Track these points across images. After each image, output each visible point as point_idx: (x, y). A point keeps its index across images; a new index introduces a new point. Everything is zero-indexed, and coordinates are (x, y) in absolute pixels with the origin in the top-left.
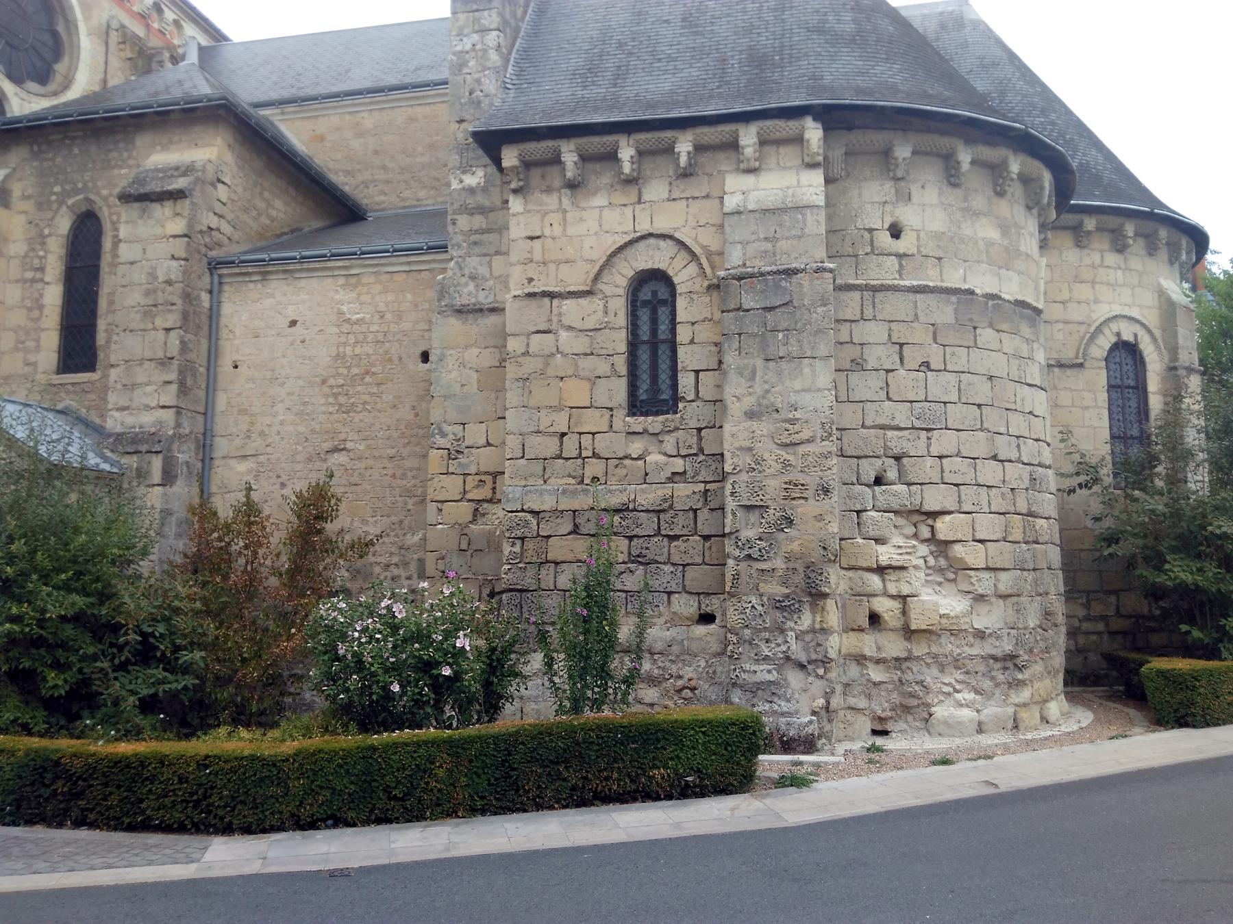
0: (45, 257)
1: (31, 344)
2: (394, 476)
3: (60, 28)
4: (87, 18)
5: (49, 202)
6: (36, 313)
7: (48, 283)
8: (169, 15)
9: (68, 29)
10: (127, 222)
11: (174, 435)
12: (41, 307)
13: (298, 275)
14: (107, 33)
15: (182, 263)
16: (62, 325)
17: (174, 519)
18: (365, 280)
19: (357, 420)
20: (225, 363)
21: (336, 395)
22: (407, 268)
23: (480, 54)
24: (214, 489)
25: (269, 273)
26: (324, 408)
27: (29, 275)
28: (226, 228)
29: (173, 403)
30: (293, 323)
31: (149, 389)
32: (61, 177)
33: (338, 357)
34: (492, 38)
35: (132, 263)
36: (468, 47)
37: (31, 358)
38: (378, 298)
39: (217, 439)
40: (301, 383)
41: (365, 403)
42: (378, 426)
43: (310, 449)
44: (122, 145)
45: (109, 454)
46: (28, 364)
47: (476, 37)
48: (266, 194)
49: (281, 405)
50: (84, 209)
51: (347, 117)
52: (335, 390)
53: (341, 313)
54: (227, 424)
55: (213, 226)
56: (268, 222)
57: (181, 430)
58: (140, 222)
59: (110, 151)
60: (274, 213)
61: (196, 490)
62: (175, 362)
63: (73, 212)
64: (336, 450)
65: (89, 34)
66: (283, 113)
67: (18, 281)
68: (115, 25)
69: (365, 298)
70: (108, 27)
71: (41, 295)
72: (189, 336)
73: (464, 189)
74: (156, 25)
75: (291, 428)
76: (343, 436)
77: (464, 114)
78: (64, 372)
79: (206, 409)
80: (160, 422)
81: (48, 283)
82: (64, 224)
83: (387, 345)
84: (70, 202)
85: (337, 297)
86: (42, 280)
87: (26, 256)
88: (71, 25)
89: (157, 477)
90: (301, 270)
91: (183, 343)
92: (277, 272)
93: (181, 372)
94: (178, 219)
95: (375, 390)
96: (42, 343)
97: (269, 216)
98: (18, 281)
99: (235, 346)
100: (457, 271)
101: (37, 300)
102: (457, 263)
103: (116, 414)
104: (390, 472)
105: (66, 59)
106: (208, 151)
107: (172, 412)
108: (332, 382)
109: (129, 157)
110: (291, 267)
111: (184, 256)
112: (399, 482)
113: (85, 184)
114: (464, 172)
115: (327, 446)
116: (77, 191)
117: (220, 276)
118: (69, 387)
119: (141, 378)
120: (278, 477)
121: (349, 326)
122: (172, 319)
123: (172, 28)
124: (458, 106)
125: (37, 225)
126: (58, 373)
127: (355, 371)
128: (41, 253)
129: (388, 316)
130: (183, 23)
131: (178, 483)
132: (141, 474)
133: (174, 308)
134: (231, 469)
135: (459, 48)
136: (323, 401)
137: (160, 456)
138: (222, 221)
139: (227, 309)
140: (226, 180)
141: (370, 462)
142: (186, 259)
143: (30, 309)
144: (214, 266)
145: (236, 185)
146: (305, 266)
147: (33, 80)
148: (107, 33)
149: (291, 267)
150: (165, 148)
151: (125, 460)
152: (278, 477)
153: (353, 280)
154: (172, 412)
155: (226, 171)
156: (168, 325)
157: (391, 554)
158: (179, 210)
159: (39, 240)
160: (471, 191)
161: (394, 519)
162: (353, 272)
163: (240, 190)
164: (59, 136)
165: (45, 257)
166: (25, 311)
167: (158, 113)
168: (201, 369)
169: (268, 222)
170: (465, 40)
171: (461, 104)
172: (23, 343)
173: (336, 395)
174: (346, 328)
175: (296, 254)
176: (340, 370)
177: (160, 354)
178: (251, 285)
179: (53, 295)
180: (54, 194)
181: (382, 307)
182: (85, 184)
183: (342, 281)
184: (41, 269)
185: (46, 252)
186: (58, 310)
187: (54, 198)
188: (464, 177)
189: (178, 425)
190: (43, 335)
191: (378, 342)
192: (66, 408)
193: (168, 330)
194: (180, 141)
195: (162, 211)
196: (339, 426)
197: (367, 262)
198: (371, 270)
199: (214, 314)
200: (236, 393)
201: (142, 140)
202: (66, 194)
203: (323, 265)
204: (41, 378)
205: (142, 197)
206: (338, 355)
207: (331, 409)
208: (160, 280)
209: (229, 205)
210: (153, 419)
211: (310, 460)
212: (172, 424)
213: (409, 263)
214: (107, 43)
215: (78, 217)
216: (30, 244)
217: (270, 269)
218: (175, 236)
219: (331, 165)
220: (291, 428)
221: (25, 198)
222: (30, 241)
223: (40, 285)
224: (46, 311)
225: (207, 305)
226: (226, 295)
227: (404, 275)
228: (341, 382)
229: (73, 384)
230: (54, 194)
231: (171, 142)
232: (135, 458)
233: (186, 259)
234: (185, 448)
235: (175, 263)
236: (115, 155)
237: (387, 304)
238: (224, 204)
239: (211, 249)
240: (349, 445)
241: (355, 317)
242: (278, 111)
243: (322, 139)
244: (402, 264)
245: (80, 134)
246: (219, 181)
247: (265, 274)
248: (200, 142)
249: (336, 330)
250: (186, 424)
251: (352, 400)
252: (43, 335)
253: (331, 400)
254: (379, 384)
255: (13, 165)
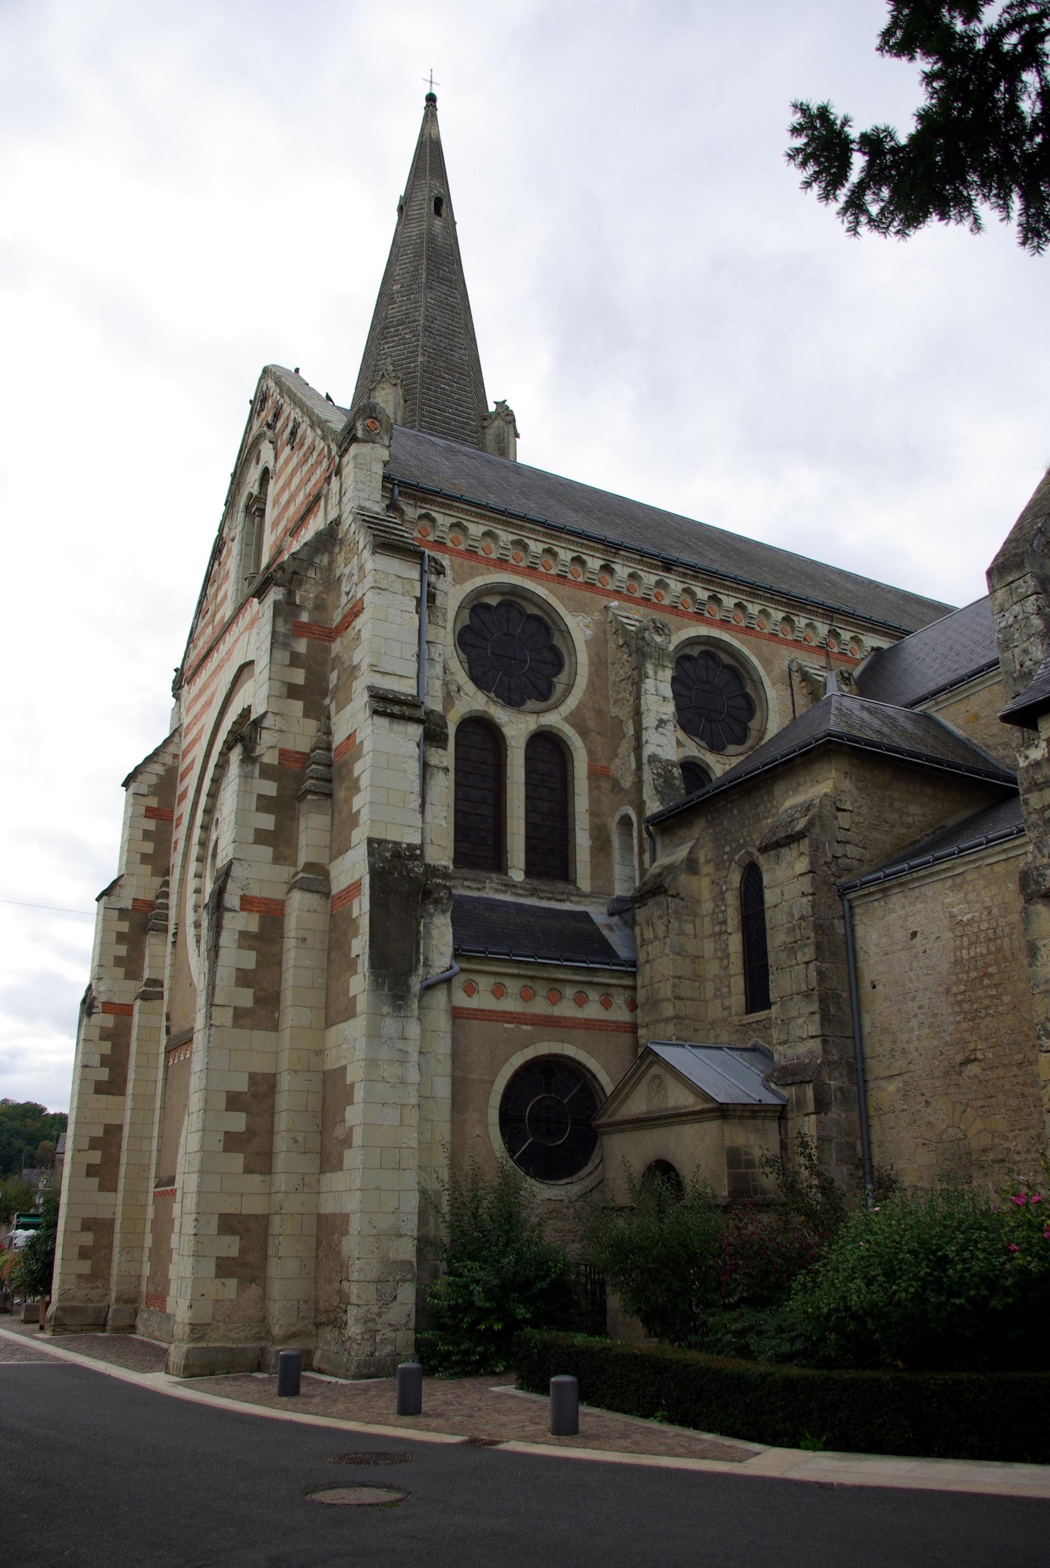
0: (725, 911)
1: (725, 990)
2: (1025, 1084)
3: (749, 690)
4: (769, 672)
5: (723, 861)
6: (725, 961)
7: (730, 934)
8: (846, 636)
9: (757, 691)
10: (767, 870)
11: (823, 1063)
12: (728, 956)
13: (912, 886)
14: (790, 677)
15: (810, 898)
16: (745, 969)
17: (833, 1145)
18: (969, 878)
19: (982, 1027)
20: (866, 985)
21: (960, 1003)
22: (1003, 857)
23: (1023, 623)
24: (872, 1112)
25: (888, 889)
26: (951, 1018)
27: (717, 929)
28: (852, 851)
29: (819, 1033)
30: (914, 935)
31: (800, 1021)
32: (729, 838)
33: (957, 962)
34: (1031, 604)
35: (775, 906)
36: (1011, 620)
37: (727, 1004)
38: (983, 893)
39: (868, 1061)
40: (928, 994)
41: (987, 1007)
42: (1003, 1031)
43: (946, 1063)
44: (766, 798)
45: (773, 1085)
46: (724, 1009)
47: (1017, 608)
48: (897, 804)
49: (915, 1020)
50: (747, 861)
51: (995, 687)
52: (959, 998)
53: (952, 916)
54: (876, 1046)
55: (838, 855)
56: (904, 830)
57: (830, 1058)
58: (777, 867)
59: (758, 805)
60: (910, 820)
61: (854, 1116)
62: (816, 992)
63: (741, 866)
64: (968, 1061)
65: (774, 684)
66: (937, 704)
67: (710, 936)
68: (794, 667)
69: (972, 896)
70: (790, 670)
71: (727, 945)
72: (825, 966)
73: (1030, 765)
74: (835, 650)
75: (926, 1043)
76: (972, 1046)
77: (1018, 688)
78: (752, 1012)
79: (854, 1032)
80: (811, 1053)
81: (730, 934)
82: (736, 878)
83: (999, 941)
84: (737, 858)
85: (947, 901)
86: (726, 931)
87: (714, 912)
88: (758, 684)
89: (811, 1107)
90: (913, 880)
91: (819, 973)
92: (893, 886)
93: (821, 1001)
94: (802, 859)
95: (994, 992)
96: (732, 989)
97: (902, 824)
98: (710, 936)
99: (874, 964)
100: (1036, 852)
101: (725, 950)
102: (1035, 844)
103: (780, 1048)
104: (1021, 1080)
105: (758, 714)
106: (822, 785)
107: (818, 1041)
108: (954, 990)
109: (772, 807)
110: (903, 879)
111: (811, 891)
112: (1031, 1090)
113: (745, 840)
114: (1028, 747)
115: (960, 1058)
116: (740, 847)
117: (849, 900)
118: (754, 1025)
119: (794, 1013)
120: (922, 1095)
121: (961, 929)
122: (809, 953)
123: (853, 645)
124: (1011, 681)
125: (718, 884)
126: (747, 1013)
127: (974, 974)
128: (723, 908)
129: (995, 911)
130: (860, 636)
131: (833, 1109)
132: (800, 1103)
133: (810, 941)
134: (883, 1090)
135: (1002, 625)
136: (950, 1011)
137: (811, 1085)
138: (848, 847)
139: (860, 931)
140: (847, 806)
141: (1001, 1072)
142: (813, 894)
143: (721, 959)
144: (843, 892)
145: (860, 808)
146: (915, 875)
147: (732, 743)
148: (790, 677)
149: (903, 879)
150: (796, 791)
151: (785, 1092)
152: (922, 1095)
153: (958, 880)
154: (818, 1041)
155: (844, 798)
156: (806, 959)
157: (1036, 1171)
158: (802, 849)
159: (719, 897)
160: (1037, 764)
161: (1033, 1132)
162: (957, 872)
163: (864, 811)
164: (723, 803)
165: (725, 911)
166: (717, 961)
167: (801, 755)
168: (844, 995)
169: (904, 830)
170: (1007, 615)
171: (1014, 679)
172: (719, 990)
173: (960, 1003)
174: (959, 931)
175: (955, 849)
176: (961, 976)
177: (804, 988)
178: (876, 904)
179: (735, 943)
180: (725, 853)
181: (988, 902)
182: (745, 840)
183: (949, 883)
184: (725, 922)
185: (726, 906)
186: (740, 956)
187: (726, 857)
188: (1028, 753)
189: (825, 1051)
190: (732, 980)
191: (990, 940)
192: (754, 1045)
193: (807, 963)
194: (805, 781)
195: (788, 854)
196: (966, 1035)
197: (967, 859)
198: (972, 866)
199: (850, 940)
200: (879, 1011)
201: (779, 789)
202: (734, 852)
203: (929, 871)
204: (735, 1020)
205: (774, 846)
206: (956, 961)
207: (958, 1019)
208: (796, 917)
209: (854, 829)
210: (806, 1049)
211: (946, 1074)
212: (820, 1052)
213: (1005, 851)
214: (791, 686)
215: (745, 869)
216: (714, 901)
217: (887, 885)
218: (802, 875)
219: (990, 741)
220: (926, 1043)
221: (708, 862)
222: (714, 899)
223: (725, 937)
224: (732, 959)
225: (841, 931)
226: (858, 918)
227: (1004, 864)
228: (962, 988)
229: (757, 1022)
230: (725, 853)
231: (799, 785)
232: (793, 1089)
233: (813, 894)
234: (836, 1074)
235: (805, 900)
236: (761, 808)
237: (992, 898)
238: (848, 830)
239: (840, 877)
240: (979, 1055)
241: (965, 919)
242: (933, 702)
243: (977, 717)
244: (999, 853)
245: (737, 796)
246: (839, 809)
247: (884, 891)
248: (820, 778)
249: (951, 935)
250: (834, 1051)
251: (975, 1006)
252: (732, 980)
253: (957, 1009)
254: (997, 985)
255: (697, 836)
